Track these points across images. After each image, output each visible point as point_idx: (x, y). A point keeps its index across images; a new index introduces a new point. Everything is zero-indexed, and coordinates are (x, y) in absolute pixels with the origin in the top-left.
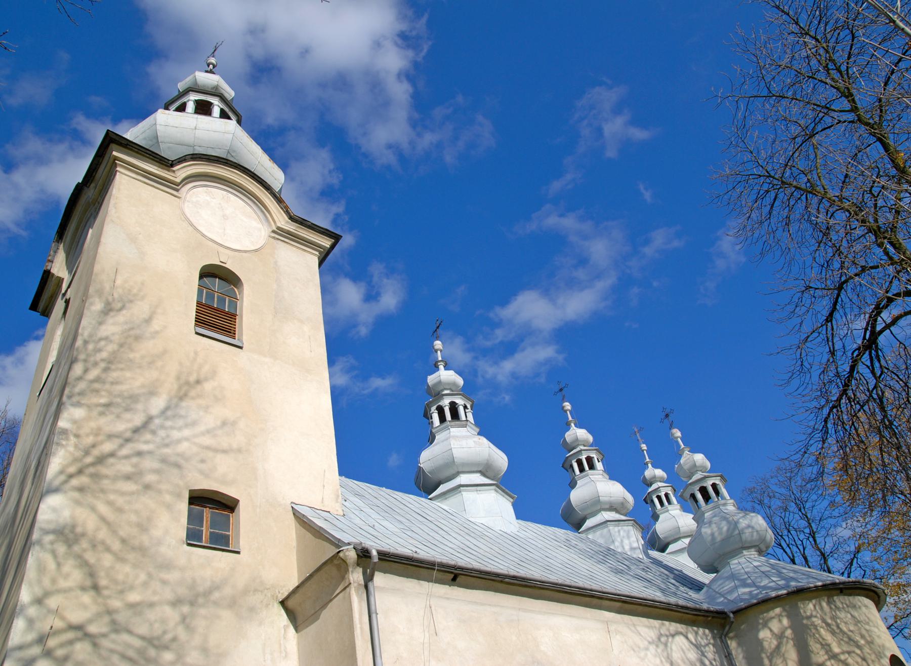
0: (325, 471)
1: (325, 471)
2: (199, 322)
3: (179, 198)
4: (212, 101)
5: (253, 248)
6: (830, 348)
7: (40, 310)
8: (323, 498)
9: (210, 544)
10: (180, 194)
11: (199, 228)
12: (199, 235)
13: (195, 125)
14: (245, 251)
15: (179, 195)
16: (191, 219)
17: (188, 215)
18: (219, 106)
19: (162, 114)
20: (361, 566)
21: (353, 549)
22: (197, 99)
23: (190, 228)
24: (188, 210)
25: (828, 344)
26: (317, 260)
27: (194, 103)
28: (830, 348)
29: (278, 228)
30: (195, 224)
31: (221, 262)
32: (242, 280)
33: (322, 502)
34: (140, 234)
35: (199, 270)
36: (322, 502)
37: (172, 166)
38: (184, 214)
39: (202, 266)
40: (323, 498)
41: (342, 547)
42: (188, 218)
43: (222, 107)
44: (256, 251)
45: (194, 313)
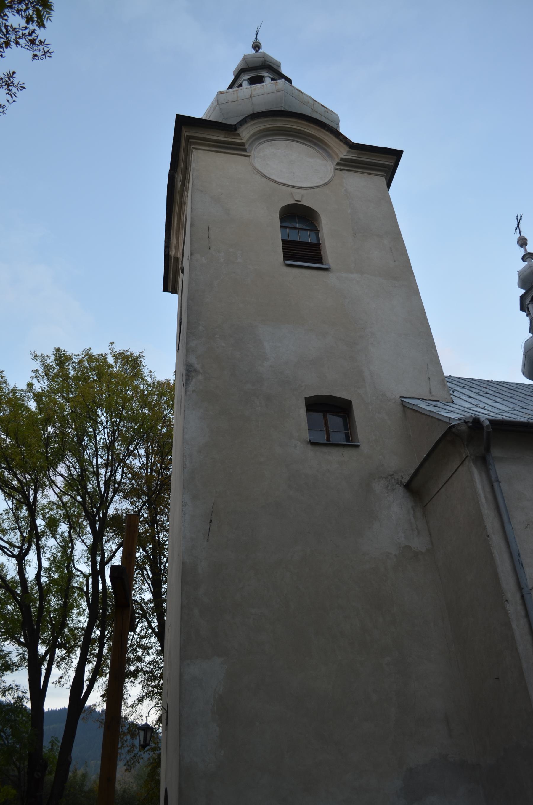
0: (428, 365)
1: (428, 365)
2: (287, 256)
3: (248, 156)
4: (263, 75)
5: (322, 183)
6: (142, 459)
7: (170, 290)
8: (430, 389)
9: (346, 442)
10: (248, 153)
11: (272, 177)
12: (272, 183)
13: (250, 94)
14: (316, 187)
15: (248, 154)
16: (262, 171)
17: (260, 169)
18: (269, 77)
19: (221, 95)
20: (464, 428)
21: (464, 423)
22: (249, 77)
23: (264, 179)
24: (258, 164)
25: (143, 462)
26: (384, 180)
27: (248, 81)
28: (142, 459)
29: (342, 159)
30: (267, 175)
31: (296, 201)
32: (317, 211)
33: (430, 393)
34: (222, 194)
35: (279, 212)
36: (430, 393)
37: (236, 129)
38: (255, 169)
39: (280, 208)
40: (430, 389)
41: (451, 423)
42: (260, 171)
43: (272, 77)
44: (326, 184)
45: (282, 250)
